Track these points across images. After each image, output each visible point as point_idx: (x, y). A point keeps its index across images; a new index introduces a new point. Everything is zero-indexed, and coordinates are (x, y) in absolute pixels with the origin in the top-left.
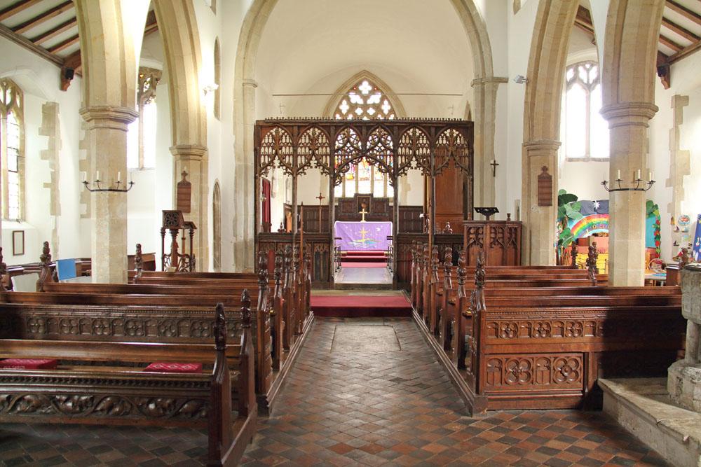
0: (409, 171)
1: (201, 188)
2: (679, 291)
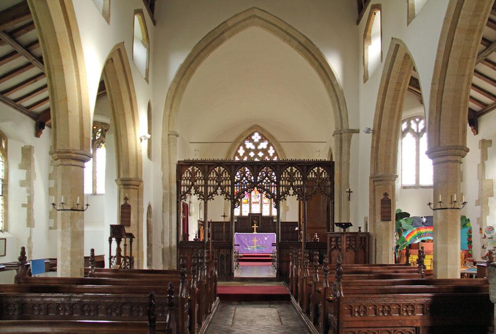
0: (288, 197)
1: (138, 209)
2: (487, 282)
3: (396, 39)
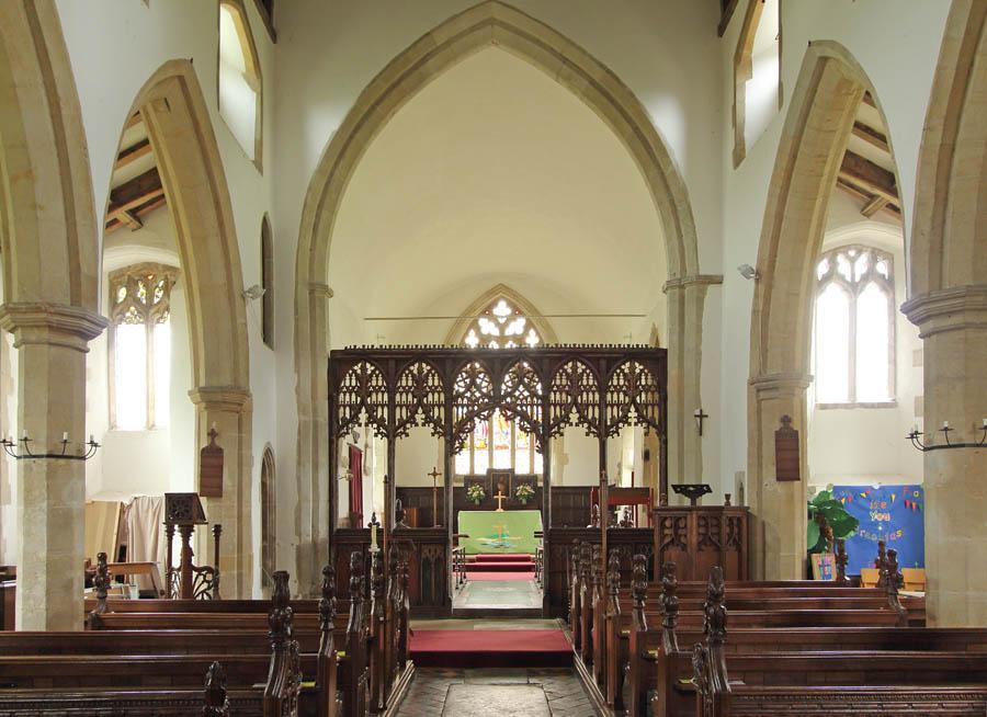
0: (567, 430)
1: (240, 457)
3: (820, 43)
